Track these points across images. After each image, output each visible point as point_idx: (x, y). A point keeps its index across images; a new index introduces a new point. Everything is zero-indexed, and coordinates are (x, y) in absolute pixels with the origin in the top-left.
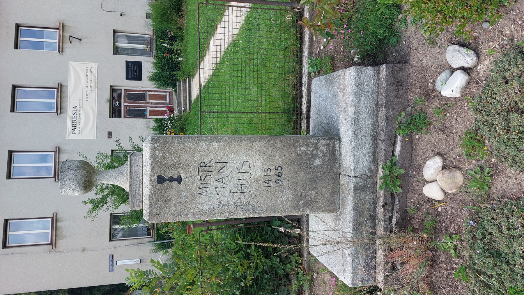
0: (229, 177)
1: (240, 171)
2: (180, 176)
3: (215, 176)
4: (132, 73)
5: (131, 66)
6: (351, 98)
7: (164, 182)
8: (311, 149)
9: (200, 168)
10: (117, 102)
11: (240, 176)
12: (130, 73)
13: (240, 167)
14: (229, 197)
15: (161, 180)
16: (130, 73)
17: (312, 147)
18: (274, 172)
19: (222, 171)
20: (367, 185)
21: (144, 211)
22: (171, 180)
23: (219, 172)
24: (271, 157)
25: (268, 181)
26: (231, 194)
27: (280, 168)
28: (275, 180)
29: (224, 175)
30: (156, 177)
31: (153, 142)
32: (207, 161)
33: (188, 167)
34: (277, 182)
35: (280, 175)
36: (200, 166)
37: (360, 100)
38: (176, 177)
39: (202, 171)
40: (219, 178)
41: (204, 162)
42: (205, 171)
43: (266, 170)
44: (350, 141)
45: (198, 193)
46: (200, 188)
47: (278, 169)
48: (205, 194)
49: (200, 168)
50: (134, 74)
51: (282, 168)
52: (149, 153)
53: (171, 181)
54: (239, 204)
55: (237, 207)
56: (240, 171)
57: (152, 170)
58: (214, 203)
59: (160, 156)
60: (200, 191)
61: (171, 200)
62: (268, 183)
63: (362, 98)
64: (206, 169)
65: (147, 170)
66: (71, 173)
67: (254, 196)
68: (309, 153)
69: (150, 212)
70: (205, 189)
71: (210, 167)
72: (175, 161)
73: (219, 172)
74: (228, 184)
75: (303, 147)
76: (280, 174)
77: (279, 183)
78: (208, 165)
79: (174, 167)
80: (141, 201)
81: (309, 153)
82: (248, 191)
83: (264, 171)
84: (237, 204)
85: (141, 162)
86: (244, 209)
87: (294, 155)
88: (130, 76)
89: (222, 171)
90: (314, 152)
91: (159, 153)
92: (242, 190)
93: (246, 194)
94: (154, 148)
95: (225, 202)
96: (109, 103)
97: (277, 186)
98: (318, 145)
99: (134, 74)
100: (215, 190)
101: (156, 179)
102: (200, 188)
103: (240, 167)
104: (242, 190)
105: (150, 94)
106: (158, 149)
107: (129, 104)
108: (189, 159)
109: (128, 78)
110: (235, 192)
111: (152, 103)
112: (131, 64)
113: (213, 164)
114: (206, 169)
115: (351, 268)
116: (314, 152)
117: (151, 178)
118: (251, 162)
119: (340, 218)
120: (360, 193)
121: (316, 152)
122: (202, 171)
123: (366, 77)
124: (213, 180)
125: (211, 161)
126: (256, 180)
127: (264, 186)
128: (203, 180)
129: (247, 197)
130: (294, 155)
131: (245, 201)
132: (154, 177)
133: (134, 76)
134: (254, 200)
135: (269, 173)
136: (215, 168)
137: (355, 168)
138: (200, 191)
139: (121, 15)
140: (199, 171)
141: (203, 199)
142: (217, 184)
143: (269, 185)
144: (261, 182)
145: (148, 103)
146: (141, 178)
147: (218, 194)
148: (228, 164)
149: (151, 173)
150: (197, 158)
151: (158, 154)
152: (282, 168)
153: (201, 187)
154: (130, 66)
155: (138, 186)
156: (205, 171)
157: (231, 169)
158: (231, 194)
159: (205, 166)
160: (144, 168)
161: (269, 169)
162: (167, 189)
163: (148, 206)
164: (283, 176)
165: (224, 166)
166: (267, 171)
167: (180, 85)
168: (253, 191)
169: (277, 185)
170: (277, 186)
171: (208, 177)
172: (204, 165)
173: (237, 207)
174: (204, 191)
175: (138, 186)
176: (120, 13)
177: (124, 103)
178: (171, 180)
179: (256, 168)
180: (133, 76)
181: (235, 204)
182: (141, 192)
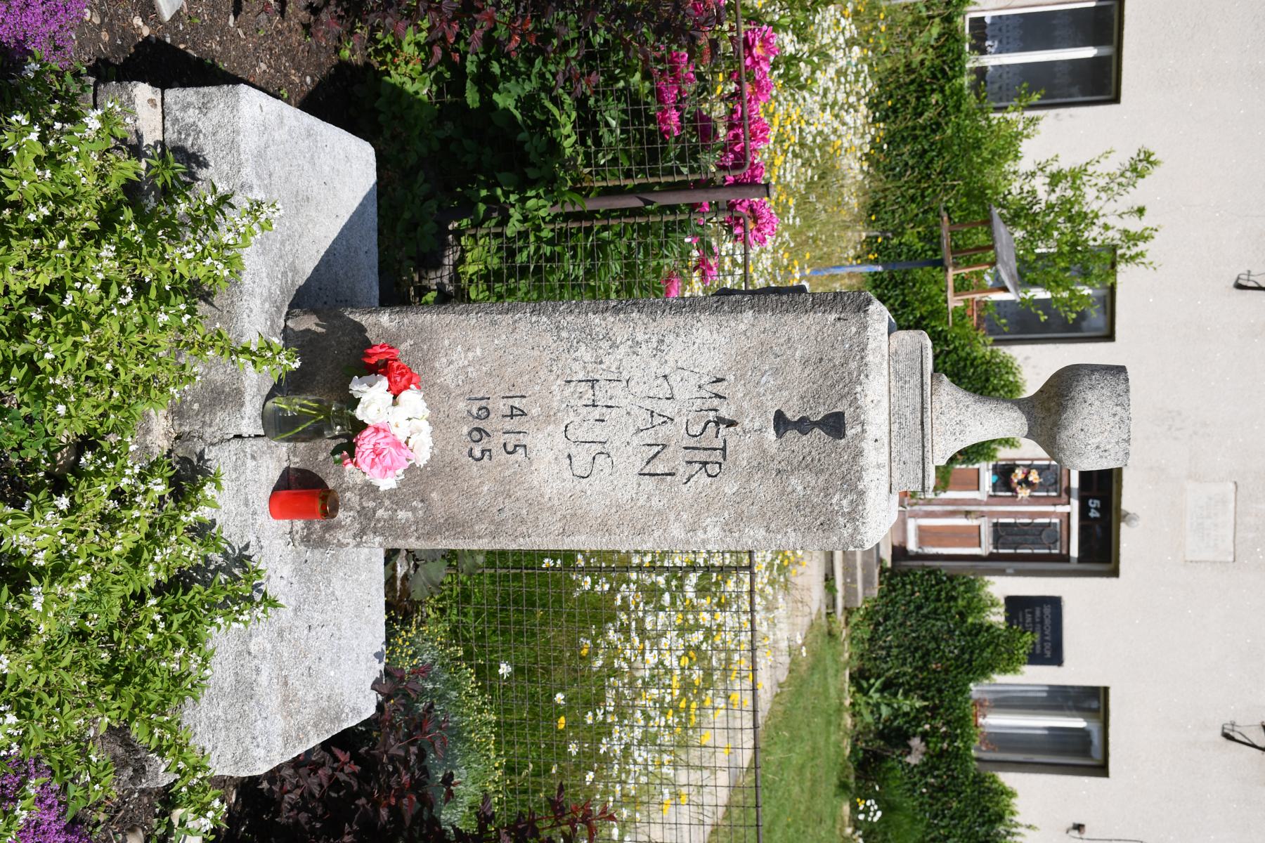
0: (632, 430)
1: (599, 448)
2: (779, 434)
3: (675, 433)
4: (1042, 622)
5: (1043, 647)
6: (263, 679)
7: (827, 417)
8: (380, 513)
9: (721, 460)
10: (1093, 514)
11: (599, 432)
12: (1047, 622)
13: (601, 460)
14: (632, 367)
15: (835, 425)
16: (1047, 622)
17: (379, 521)
18: (495, 443)
19: (656, 449)
20: (203, 407)
21: (884, 328)
22: (803, 425)
23: (664, 446)
24: (505, 488)
25: (512, 416)
26: (625, 375)
27: (477, 454)
28: (492, 416)
29: (648, 437)
30: (850, 432)
31: (859, 537)
32: (703, 479)
33: (755, 464)
34: (483, 413)
35: (475, 433)
36: (720, 464)
37: (237, 674)
38: (791, 434)
39: (715, 449)
40: (663, 428)
41: (709, 476)
42: (705, 449)
43: (521, 451)
44: (261, 548)
45: (725, 383)
46: (721, 397)
47: (483, 452)
48: (706, 379)
49: (721, 460)
50: (1033, 617)
51: (470, 455)
52: (867, 506)
53: (803, 420)
54: (601, 343)
55: (606, 337)
56: (599, 448)
57: (860, 453)
58: (677, 352)
59: (837, 497)
60: (719, 388)
61: (805, 362)
62: (512, 407)
63: (231, 679)
64: (702, 456)
65: (874, 456)
66: (1099, 439)
67: (555, 368)
68: (387, 503)
69: (866, 328)
70: (703, 393)
71: (689, 463)
72: (793, 480)
73: (664, 446)
74: (636, 408)
75: (407, 520)
76: (476, 435)
77: (480, 409)
78: (697, 466)
79: (795, 463)
80: (893, 356)
81: (387, 503)
82: (573, 384)
83: (525, 446)
84: (606, 345)
85: (896, 475)
86: (589, 336)
87: (434, 495)
88: (1047, 610)
89: (656, 449)
90: (371, 504)
91: (838, 504)
92: (593, 387)
93: (581, 376)
94: (854, 520)
95: (644, 350)
96: (1126, 506)
97: (482, 399)
98: (357, 526)
99: (1033, 617)
100: (676, 391)
101: (848, 426)
102: (721, 397)
103: (601, 460)
104: (593, 387)
105: (973, 546)
106: (843, 515)
107: (1051, 509)
108: (754, 485)
109: (1054, 604)
110: (616, 383)
111: (967, 514)
112: (1043, 654)
113: (683, 470)
114: (702, 456)
115: (242, 146)
116: (371, 504)
117: (863, 431)
118: (567, 475)
119: (282, 293)
120: (223, 384)
121: (365, 504)
122: (715, 449)
123: (220, 745)
124: (681, 421)
125: (689, 480)
126: (549, 417)
127: (524, 401)
128: (709, 422)
129: (576, 366)
130: (434, 495)
131: (584, 353)
132: (853, 431)
133: (1033, 613)
134: (553, 356)
135: (512, 440)
136: (675, 459)
137: (244, 464)
138: (719, 388)
139: (1079, 827)
140: (724, 449)
141: (711, 363)
142: (669, 409)
143: (511, 402)
144: (535, 411)
145: (982, 515)
146: (895, 427)
147: (665, 376)
148: (637, 470)
149: (863, 444)
150: (730, 487)
151: (845, 502)
152: (470, 455)
153: (716, 402)
154: (1048, 646)
155: (904, 403)
156: (705, 449)
157: (630, 458)
158: (625, 375)
159: (705, 464)
160: (884, 458)
161: (509, 453)
162: (816, 396)
163: (872, 345)
164: (465, 430)
165: (648, 463)
166: (516, 446)
167: (867, 582)
168: (559, 382)
169: (483, 403)
170: (482, 399)
171: (696, 429)
172: (708, 466)
173: (606, 337)
174: (709, 388)
175: (904, 403)
176: (1085, 836)
177: (1069, 514)
178: (803, 425)
179: (550, 456)
180: (1038, 613)
181: (614, 346)
182: (893, 383)
